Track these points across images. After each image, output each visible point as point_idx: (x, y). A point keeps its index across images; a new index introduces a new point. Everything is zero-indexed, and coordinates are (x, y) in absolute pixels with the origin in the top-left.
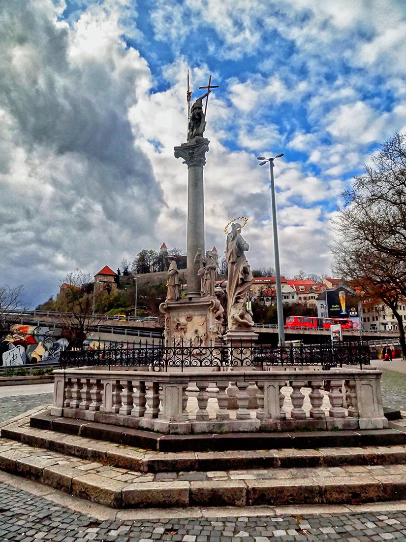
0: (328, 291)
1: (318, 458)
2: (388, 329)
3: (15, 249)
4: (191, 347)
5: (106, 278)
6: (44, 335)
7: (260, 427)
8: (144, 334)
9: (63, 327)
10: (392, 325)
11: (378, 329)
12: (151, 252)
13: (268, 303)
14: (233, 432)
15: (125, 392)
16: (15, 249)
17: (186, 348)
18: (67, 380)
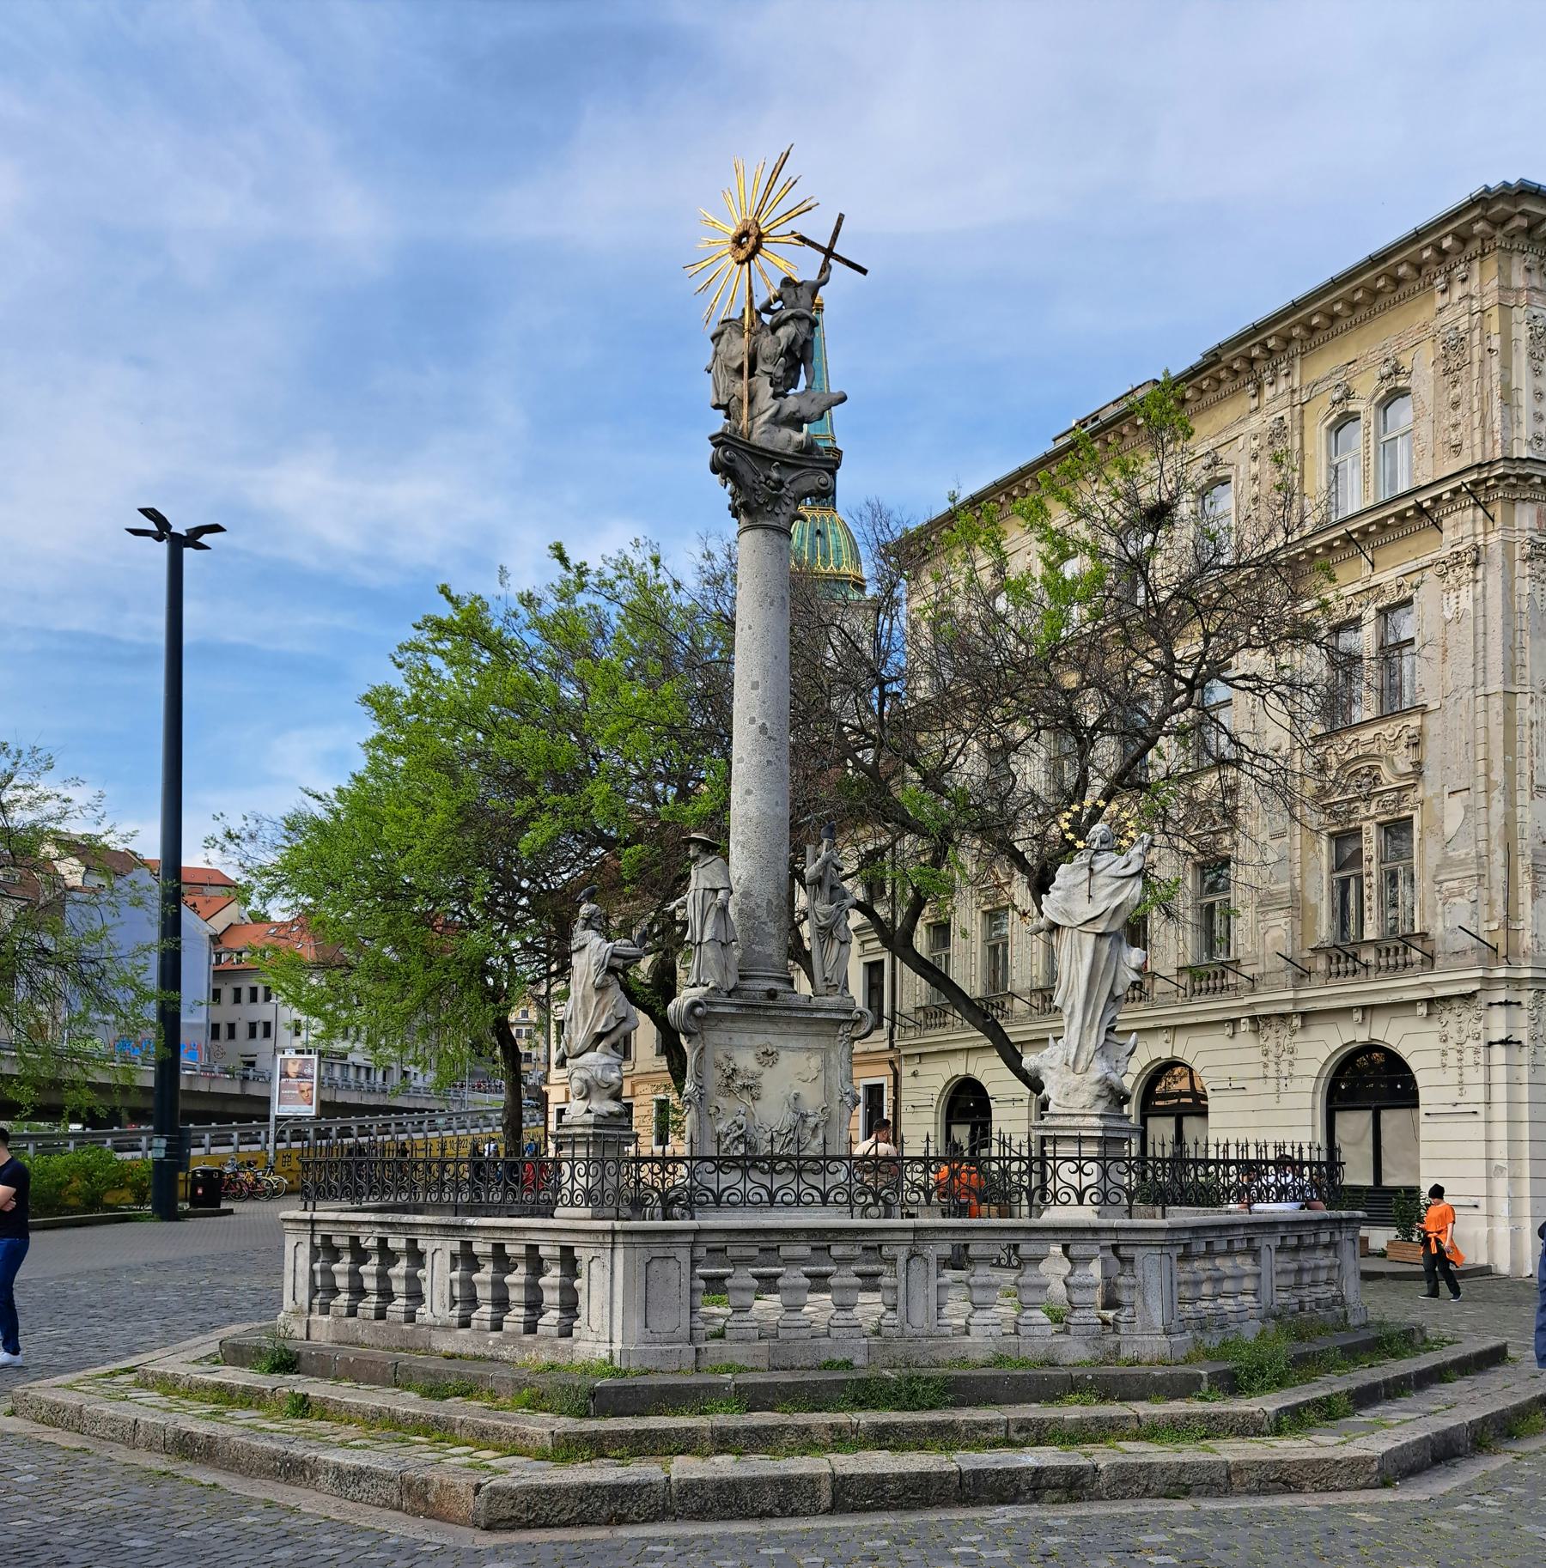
3: (532, 639)
4: (1080, 1159)
15: (485, 1274)
16: (532, 639)
18: (318, 1240)
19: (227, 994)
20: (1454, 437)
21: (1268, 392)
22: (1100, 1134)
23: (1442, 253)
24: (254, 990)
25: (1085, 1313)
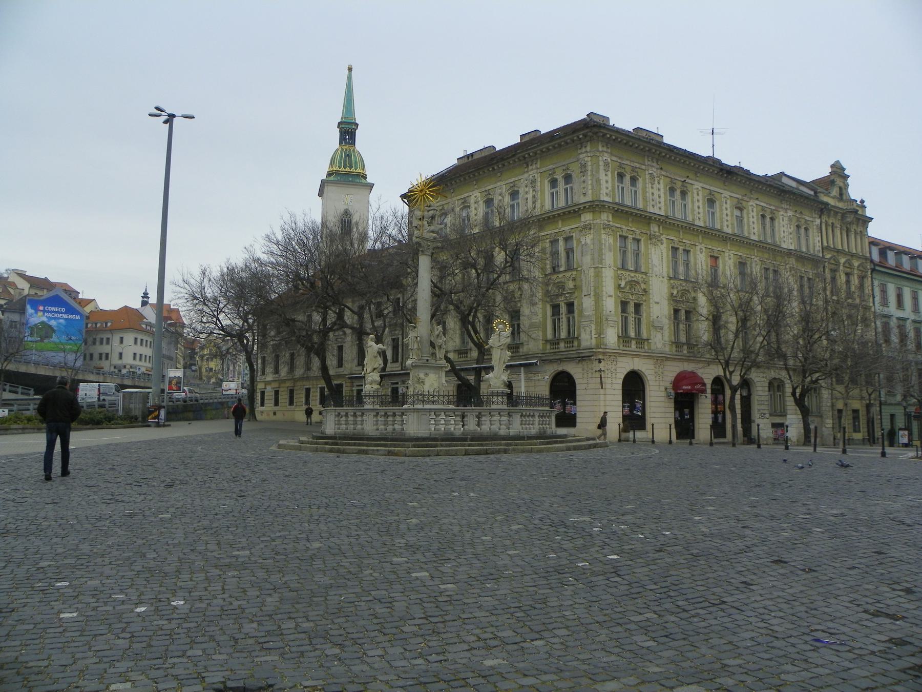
20: (584, 191)
21: (530, 168)
23: (580, 139)
24: (102, 339)
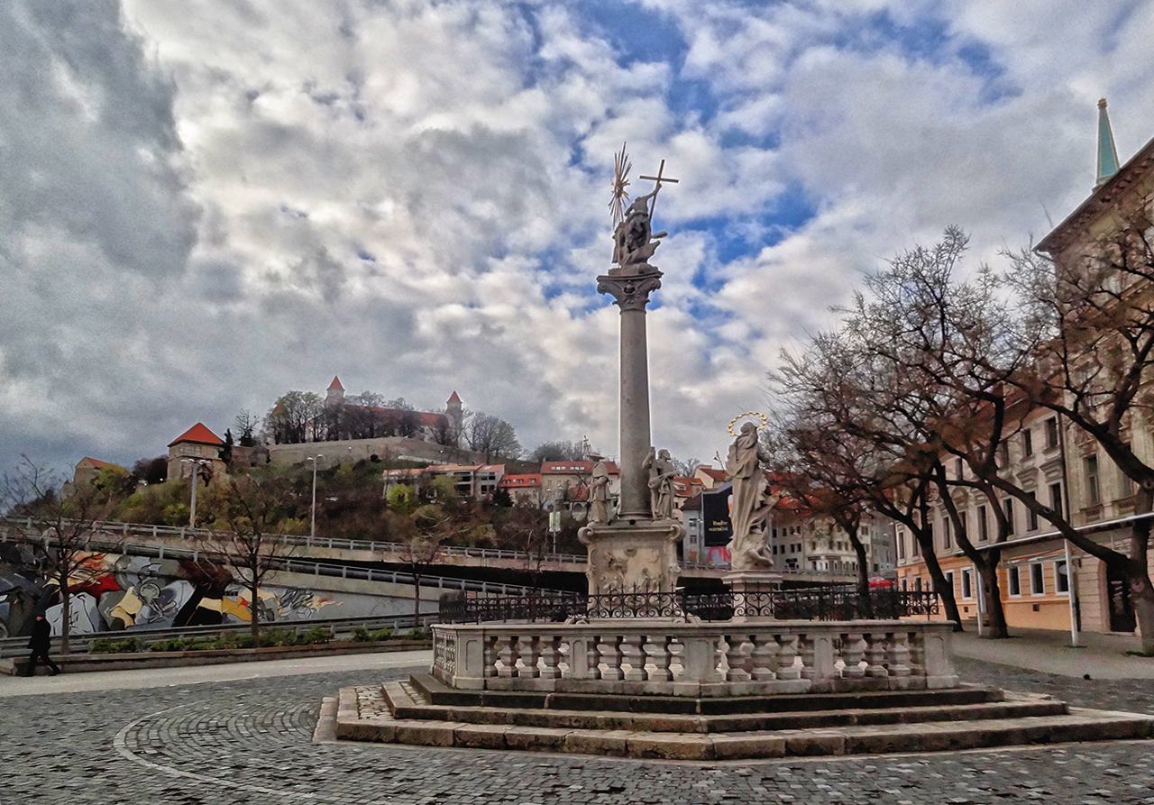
0: (706, 493)
1: (898, 715)
2: (818, 567)
5: (198, 449)
6: (139, 574)
7: (811, 687)
8: (356, 572)
9: (185, 561)
10: (827, 561)
11: (801, 567)
12: (310, 397)
13: (580, 514)
14: (778, 694)
17: (627, 595)
19: (779, 532)
22: (740, 581)
25: (56, 648)
